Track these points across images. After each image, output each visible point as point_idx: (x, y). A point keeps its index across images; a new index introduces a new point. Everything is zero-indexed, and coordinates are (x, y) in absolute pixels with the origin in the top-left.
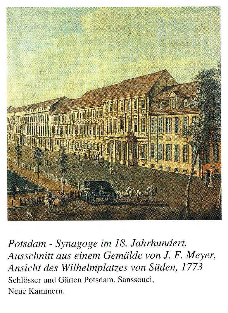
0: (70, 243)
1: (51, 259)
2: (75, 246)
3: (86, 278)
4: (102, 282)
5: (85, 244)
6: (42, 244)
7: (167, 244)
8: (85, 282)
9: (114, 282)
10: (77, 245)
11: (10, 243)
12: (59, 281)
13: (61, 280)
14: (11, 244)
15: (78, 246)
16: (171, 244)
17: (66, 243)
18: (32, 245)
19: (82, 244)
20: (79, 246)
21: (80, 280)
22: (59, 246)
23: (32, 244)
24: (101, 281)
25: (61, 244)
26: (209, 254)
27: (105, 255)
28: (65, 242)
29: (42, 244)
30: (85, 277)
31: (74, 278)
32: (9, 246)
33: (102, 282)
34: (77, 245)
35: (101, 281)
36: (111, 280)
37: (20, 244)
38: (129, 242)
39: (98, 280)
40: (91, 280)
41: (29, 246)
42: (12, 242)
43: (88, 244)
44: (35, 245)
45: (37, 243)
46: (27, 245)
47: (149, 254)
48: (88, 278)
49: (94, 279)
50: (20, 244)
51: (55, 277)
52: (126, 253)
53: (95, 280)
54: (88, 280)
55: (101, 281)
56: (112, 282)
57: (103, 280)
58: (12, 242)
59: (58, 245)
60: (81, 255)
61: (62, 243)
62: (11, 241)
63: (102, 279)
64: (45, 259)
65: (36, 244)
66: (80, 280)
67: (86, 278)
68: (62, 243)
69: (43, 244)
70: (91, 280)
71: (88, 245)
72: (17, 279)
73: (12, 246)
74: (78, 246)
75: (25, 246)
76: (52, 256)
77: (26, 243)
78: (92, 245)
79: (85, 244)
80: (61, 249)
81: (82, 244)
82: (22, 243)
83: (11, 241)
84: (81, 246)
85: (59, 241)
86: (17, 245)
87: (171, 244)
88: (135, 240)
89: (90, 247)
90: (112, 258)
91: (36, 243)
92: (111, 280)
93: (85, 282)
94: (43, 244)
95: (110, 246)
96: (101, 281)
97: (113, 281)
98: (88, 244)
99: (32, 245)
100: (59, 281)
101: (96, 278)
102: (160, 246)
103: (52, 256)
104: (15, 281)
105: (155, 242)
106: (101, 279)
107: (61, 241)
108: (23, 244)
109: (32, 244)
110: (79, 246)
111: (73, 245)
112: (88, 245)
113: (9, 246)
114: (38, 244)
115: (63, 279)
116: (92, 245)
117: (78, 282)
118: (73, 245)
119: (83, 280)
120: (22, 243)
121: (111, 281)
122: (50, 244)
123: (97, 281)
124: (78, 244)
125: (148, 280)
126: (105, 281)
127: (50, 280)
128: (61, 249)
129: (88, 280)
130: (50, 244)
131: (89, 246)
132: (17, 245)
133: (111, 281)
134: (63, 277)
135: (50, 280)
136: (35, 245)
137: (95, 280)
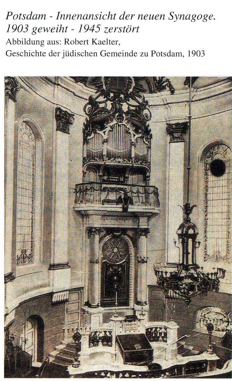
0: (184, 15)
1: (66, 32)
2: (189, 19)
3: (154, 52)
4: (170, 56)
5: (200, 17)
6: (42, 16)
7: (82, 17)
8: (152, 56)
9: (183, 56)
10: (191, 18)
11: (8, 15)
12: (101, 55)
13: (103, 54)
14: (9, 16)
15: (193, 19)
16: (123, 17)
17: (180, 16)
18: (32, 17)
19: (197, 16)
20: (205, 19)
21: (95, 54)
22: (173, 18)
23: (31, 17)
24: (169, 55)
25: (174, 17)
26: (113, 28)
27: (21, 30)
28: (179, 15)
29: (42, 16)
30: (152, 51)
31: (42, 52)
32: (7, 19)
33: (170, 56)
34: (191, 18)
35: (169, 55)
36: (180, 54)
37: (19, 17)
38: (175, 14)
39: (166, 54)
40: (158, 54)
41: (28, 18)
42: (10, 14)
43: (203, 16)
44: (34, 18)
45: (37, 15)
46: (26, 17)
47: (50, 28)
48: (155, 52)
49: (161, 52)
50: (19, 17)
51: (132, 51)
52: (128, 27)
53: (163, 54)
54: (156, 53)
55: (169, 55)
56: (181, 56)
57: (171, 54)
58: (10, 14)
59: (171, 18)
60: (58, 28)
61: (176, 15)
62: (9, 12)
63: (170, 53)
64: (57, 32)
65: (35, 16)
66: (95, 54)
67: (154, 52)
68: (176, 15)
69: (43, 16)
70: (158, 54)
71: (203, 17)
72: (85, 53)
73: (10, 18)
74: (193, 19)
75: (24, 18)
76: (138, 29)
77: (25, 15)
78: (207, 18)
79: (200, 17)
80: (174, 21)
81: (197, 16)
82: (21, 15)
83: (9, 12)
84: (196, 18)
85: (172, 14)
86: (15, 17)
87: (123, 17)
88: (59, 13)
89: (205, 20)
90: (51, 31)
91: (35, 16)
92: (180, 54)
93: (152, 56)
94: (43, 16)
95: (163, 19)
96: (169, 55)
97: (182, 55)
98: (203, 16)
99: (32, 17)
100: (101, 55)
101: (163, 52)
102: (152, 19)
103: (138, 29)
104: (82, 54)
105: (112, 15)
106: (72, 53)
107: (175, 14)
108: (22, 17)
109: (31, 17)
110: (205, 19)
111: (187, 17)
112: (203, 17)
113: (7, 19)
114: (66, 16)
115: (105, 53)
116: (207, 18)
117: (112, 56)
118: (187, 17)
119: (150, 54)
120: (21, 15)
121: (180, 55)
122: (50, 17)
123: (165, 55)
124: (192, 17)
125: (33, 54)
126: (173, 55)
127: (127, 54)
128: (174, 21)
129: (156, 53)
130: (50, 17)
131: (204, 19)
132: (15, 17)
133: (180, 55)
134: (11, 51)
135: (127, 54)
136: (34, 18)
137: (163, 54)
